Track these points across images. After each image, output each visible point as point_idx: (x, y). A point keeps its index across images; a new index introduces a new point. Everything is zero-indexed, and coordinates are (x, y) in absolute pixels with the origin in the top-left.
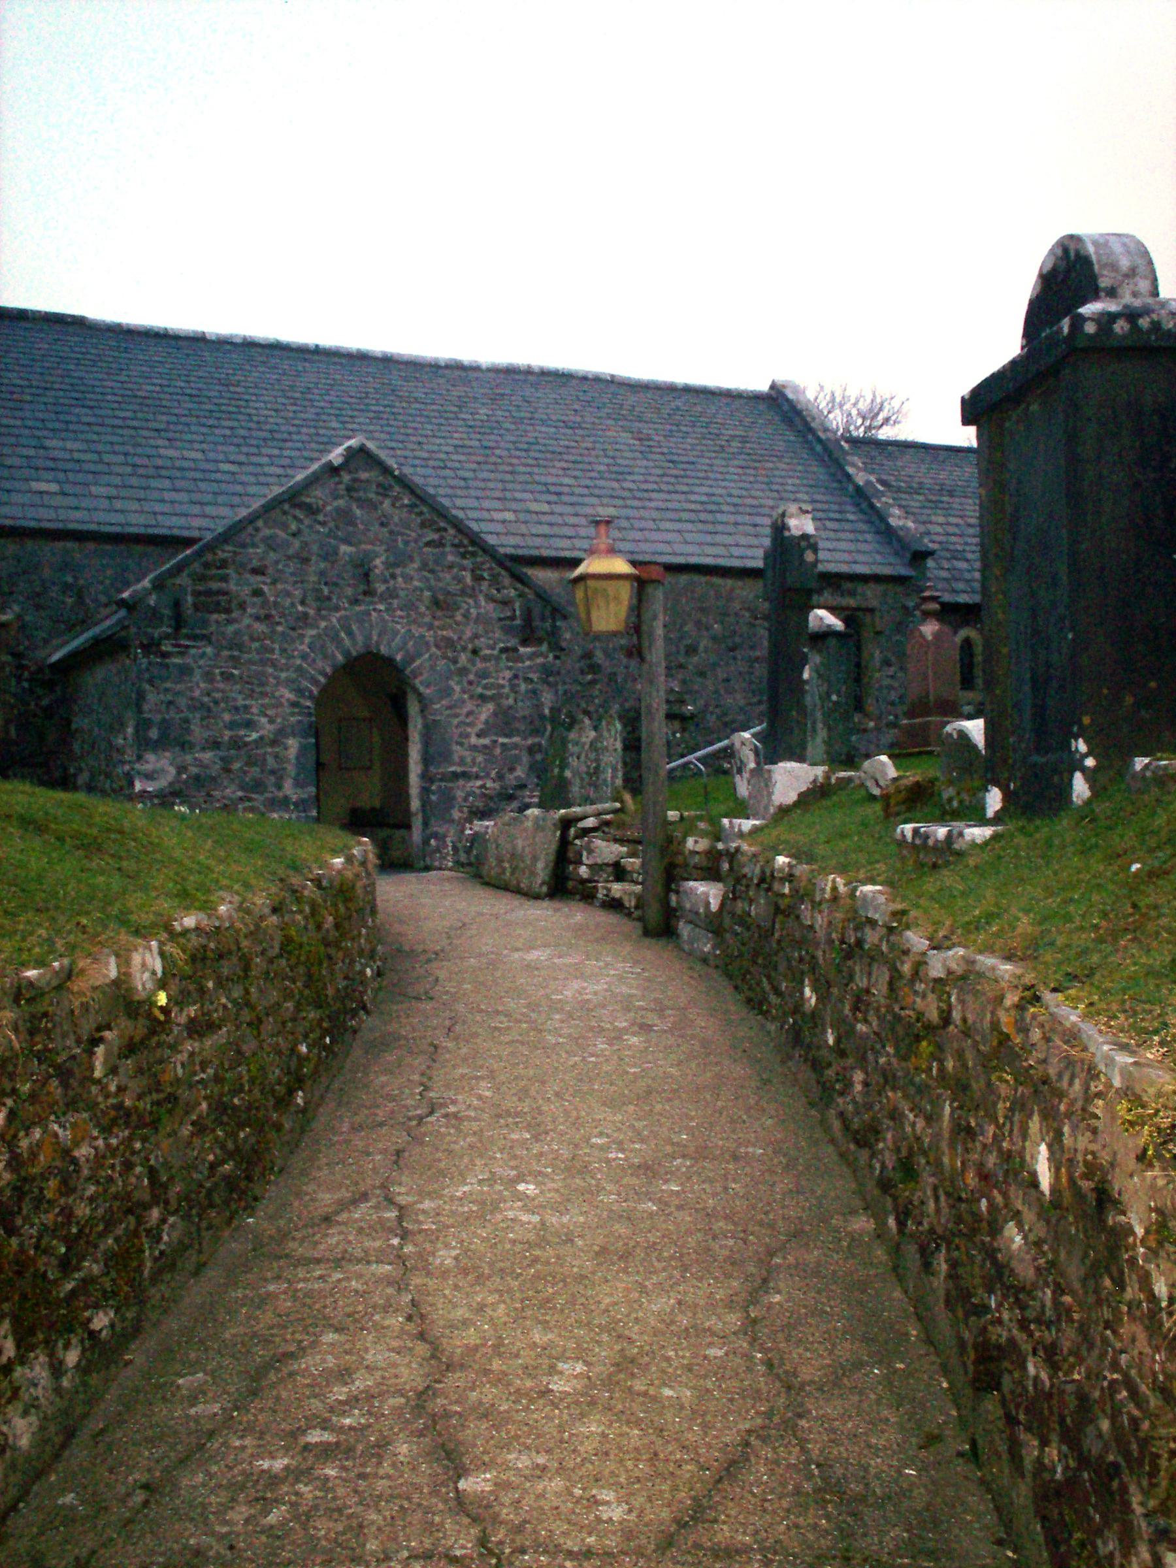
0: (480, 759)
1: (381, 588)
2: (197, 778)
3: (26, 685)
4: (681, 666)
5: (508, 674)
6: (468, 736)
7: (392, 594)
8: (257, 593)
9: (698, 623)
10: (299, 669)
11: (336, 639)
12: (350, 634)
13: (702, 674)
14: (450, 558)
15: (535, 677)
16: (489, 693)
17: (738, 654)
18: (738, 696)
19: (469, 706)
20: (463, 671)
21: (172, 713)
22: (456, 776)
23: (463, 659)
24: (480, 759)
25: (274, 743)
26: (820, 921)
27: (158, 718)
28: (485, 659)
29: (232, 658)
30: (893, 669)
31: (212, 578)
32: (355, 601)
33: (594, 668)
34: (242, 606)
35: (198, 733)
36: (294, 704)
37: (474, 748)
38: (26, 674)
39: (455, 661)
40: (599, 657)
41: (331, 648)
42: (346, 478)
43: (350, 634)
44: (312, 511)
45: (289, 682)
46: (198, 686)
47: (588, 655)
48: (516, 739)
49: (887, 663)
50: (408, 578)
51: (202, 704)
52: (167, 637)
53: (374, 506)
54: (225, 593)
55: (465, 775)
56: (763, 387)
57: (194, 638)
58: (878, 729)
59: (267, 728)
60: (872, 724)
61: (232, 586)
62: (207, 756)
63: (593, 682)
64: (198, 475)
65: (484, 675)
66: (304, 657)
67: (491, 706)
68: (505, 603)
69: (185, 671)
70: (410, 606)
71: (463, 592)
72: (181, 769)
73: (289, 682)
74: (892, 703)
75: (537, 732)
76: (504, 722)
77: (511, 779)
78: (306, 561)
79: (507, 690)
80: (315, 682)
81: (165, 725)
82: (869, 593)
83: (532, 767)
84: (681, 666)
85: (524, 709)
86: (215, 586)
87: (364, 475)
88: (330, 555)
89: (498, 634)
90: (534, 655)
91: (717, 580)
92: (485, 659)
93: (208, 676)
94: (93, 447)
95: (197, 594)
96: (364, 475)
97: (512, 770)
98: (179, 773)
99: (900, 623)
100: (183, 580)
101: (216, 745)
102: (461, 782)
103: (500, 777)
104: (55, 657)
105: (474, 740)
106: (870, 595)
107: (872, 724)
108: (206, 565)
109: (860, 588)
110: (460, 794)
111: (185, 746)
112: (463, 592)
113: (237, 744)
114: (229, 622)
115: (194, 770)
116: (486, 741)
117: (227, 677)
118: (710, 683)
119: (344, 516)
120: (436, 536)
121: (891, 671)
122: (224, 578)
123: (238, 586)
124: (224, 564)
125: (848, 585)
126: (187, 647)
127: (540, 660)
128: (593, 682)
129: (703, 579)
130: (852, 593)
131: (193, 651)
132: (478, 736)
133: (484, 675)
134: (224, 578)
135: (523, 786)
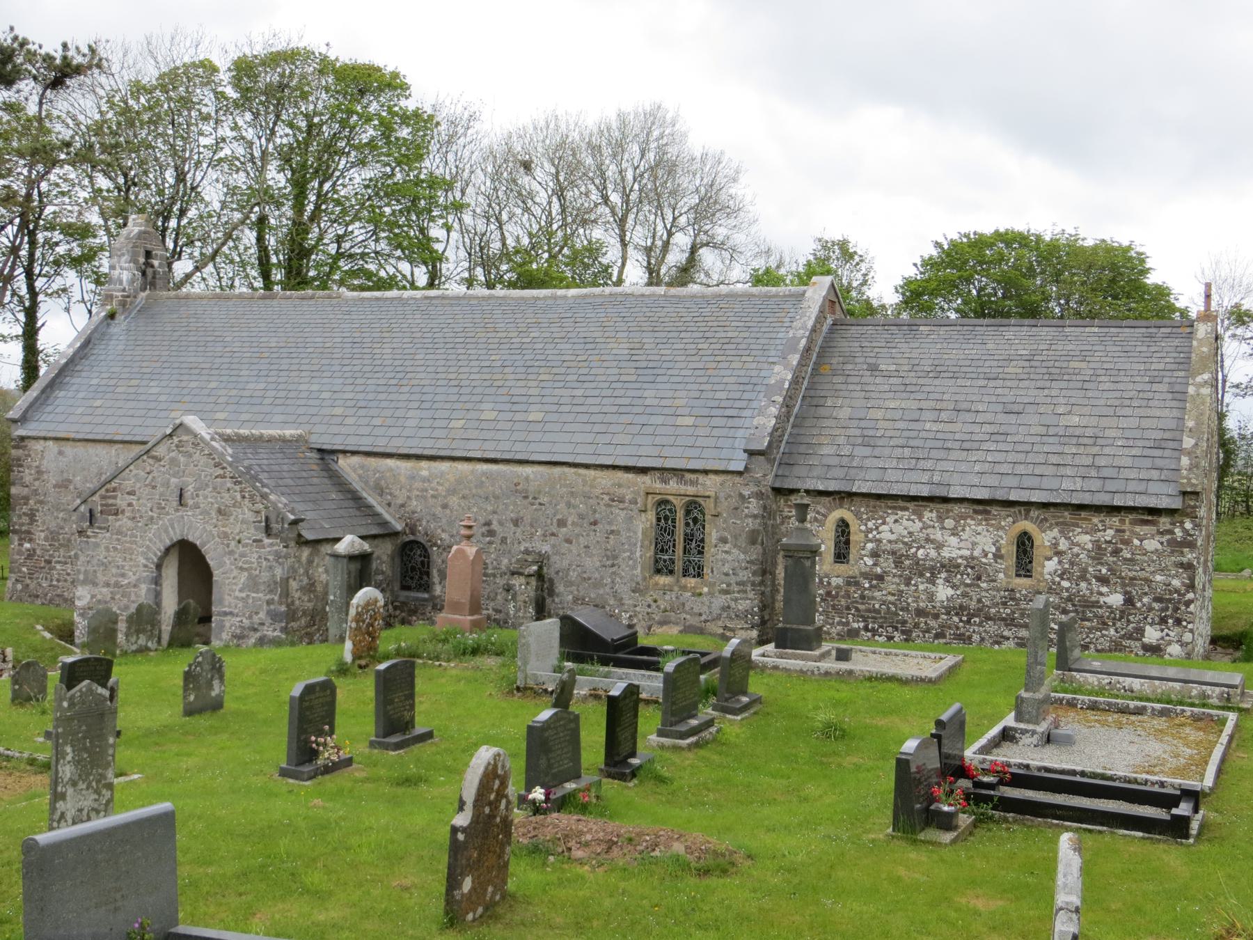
0: (240, 605)
1: (190, 502)
4: (553, 534)
5: (256, 556)
6: (234, 591)
7: (197, 506)
8: (130, 505)
9: (569, 505)
10: (148, 547)
11: (166, 531)
12: (173, 528)
13: (569, 541)
14: (229, 485)
15: (271, 558)
16: (246, 566)
17: (598, 527)
18: (595, 559)
19: (235, 572)
20: (231, 553)
22: (226, 614)
23: (233, 543)
24: (240, 605)
25: (135, 586)
28: (245, 545)
29: (118, 540)
30: (728, 545)
31: (109, 497)
32: (177, 510)
33: (491, 533)
34: (123, 512)
35: (101, 578)
36: (145, 566)
37: (237, 598)
39: (228, 546)
40: (495, 526)
41: (164, 536)
42: (176, 439)
43: (173, 528)
44: (158, 459)
45: (143, 553)
46: (101, 553)
47: (488, 524)
48: (261, 595)
49: (724, 540)
50: (206, 497)
53: (190, 456)
55: (231, 613)
57: (100, 528)
58: (711, 594)
59: (133, 578)
60: (706, 590)
61: (118, 501)
62: (105, 590)
63: (490, 543)
65: (243, 555)
66: (150, 540)
67: (246, 574)
68: (258, 512)
69: (97, 545)
70: (205, 513)
71: (234, 506)
72: (93, 597)
73: (143, 553)
74: (727, 574)
75: (271, 592)
76: (253, 584)
77: (256, 619)
78: (154, 487)
79: (255, 565)
80: (155, 555)
82: (708, 483)
83: (268, 613)
84: (553, 534)
85: (265, 576)
86: (110, 501)
87: (185, 438)
88: (167, 485)
89: (252, 531)
90: (272, 545)
91: (582, 471)
92: (245, 545)
93: (107, 549)
95: (102, 505)
96: (185, 438)
97: (257, 613)
99: (736, 509)
100: (96, 498)
101: (107, 585)
102: (229, 617)
103: (250, 617)
105: (237, 593)
106: (710, 485)
107: (706, 590)
108: (107, 491)
109: (701, 478)
110: (228, 625)
112: (234, 506)
113: (117, 585)
114: (117, 520)
116: (244, 595)
117: (115, 549)
118: (573, 548)
119: (173, 461)
120: (221, 472)
121: (727, 547)
123: (121, 501)
124: (114, 490)
125: (688, 476)
127: (276, 548)
128: (490, 543)
129: (573, 470)
130: (692, 483)
132: (240, 591)
133: (243, 555)
134: (115, 497)
135: (263, 624)
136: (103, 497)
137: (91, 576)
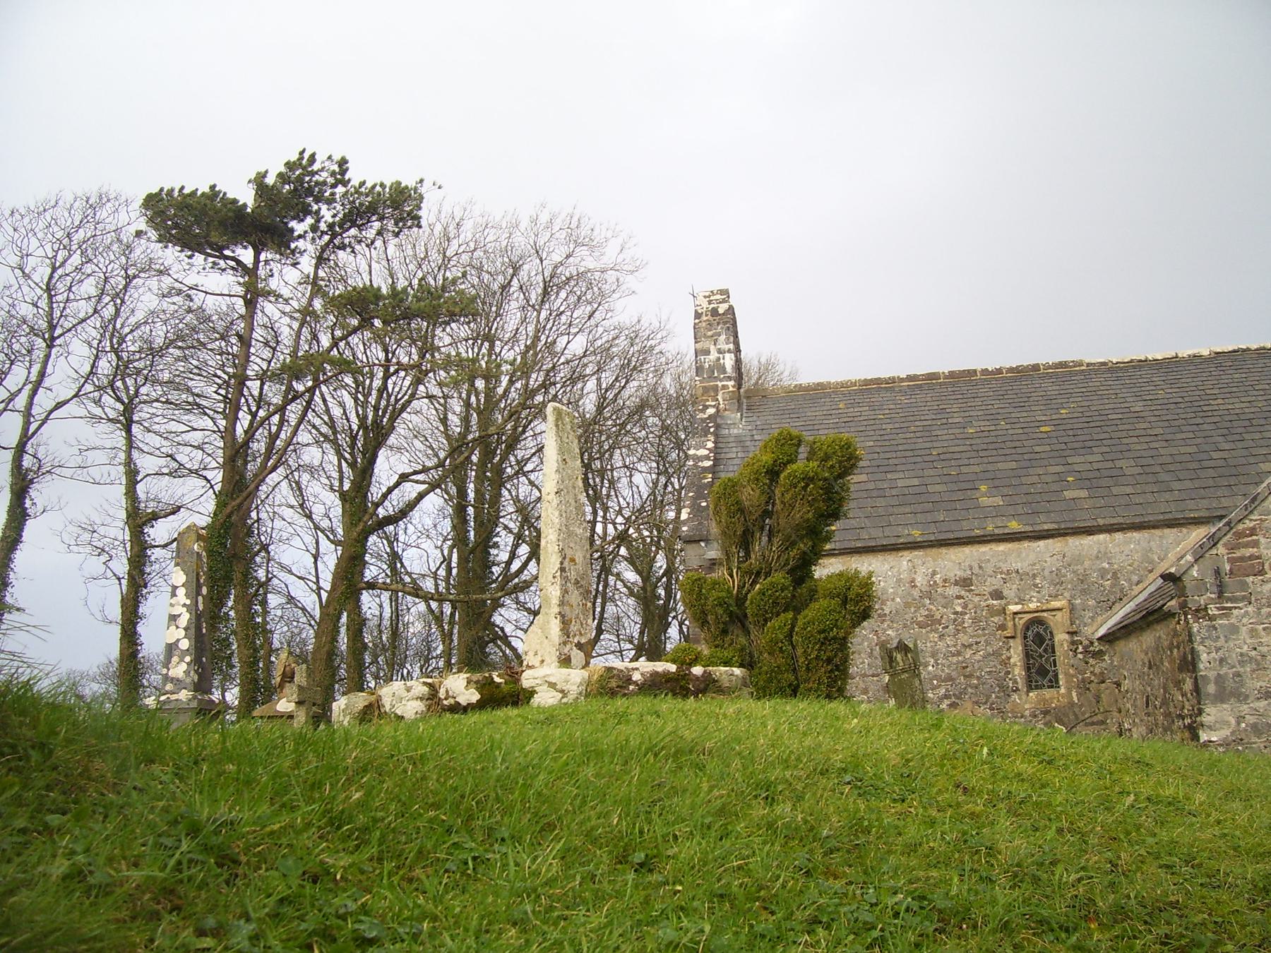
2: (1254, 727)
3: (1080, 656)
21: (1224, 670)
26: (517, 754)
27: (1212, 675)
38: (1080, 649)
51: (1251, 658)
52: (1212, 601)
54: (1258, 557)
56: (204, 188)
64: (1195, 465)
69: (1234, 629)
72: (1240, 719)
81: (1220, 679)
94: (1148, 470)
98: (1238, 723)
100: (1221, 549)
104: (1102, 632)
111: (1242, 698)
115: (1251, 719)
122: (1256, 544)
124: (1253, 532)
126: (1230, 609)
131: (1235, 612)
134: (1256, 544)
136: (1232, 548)
137: (1230, 684)
